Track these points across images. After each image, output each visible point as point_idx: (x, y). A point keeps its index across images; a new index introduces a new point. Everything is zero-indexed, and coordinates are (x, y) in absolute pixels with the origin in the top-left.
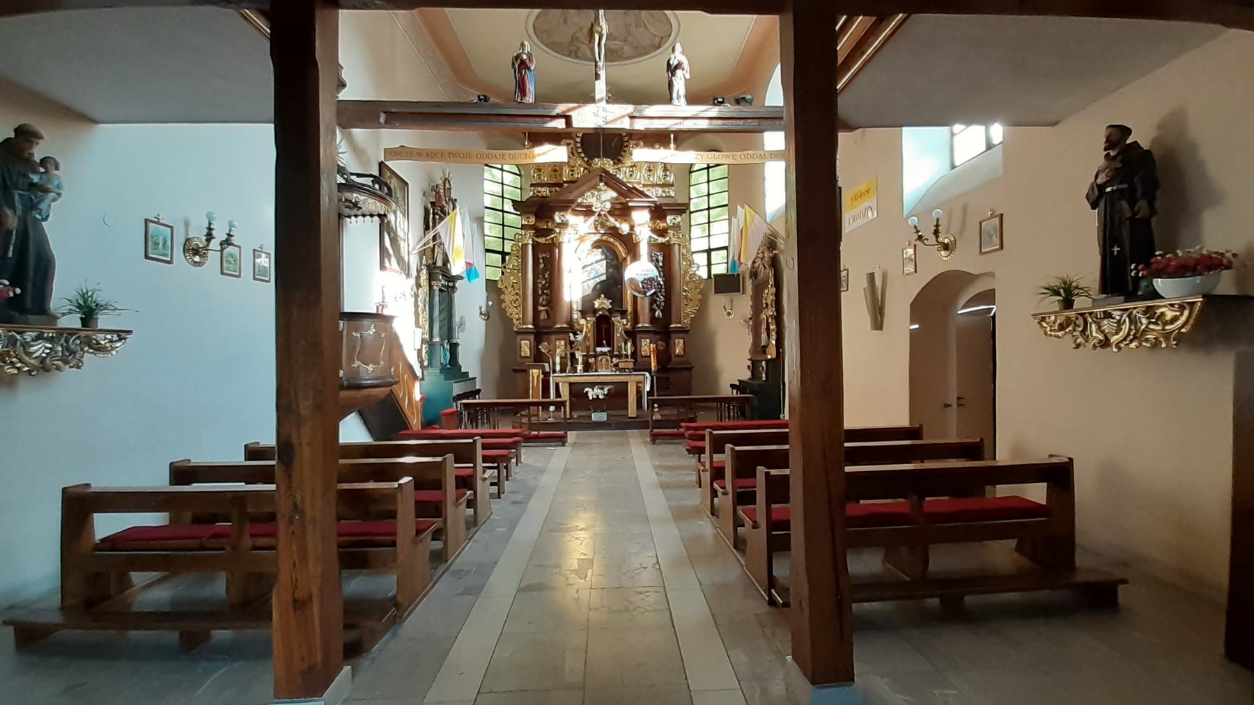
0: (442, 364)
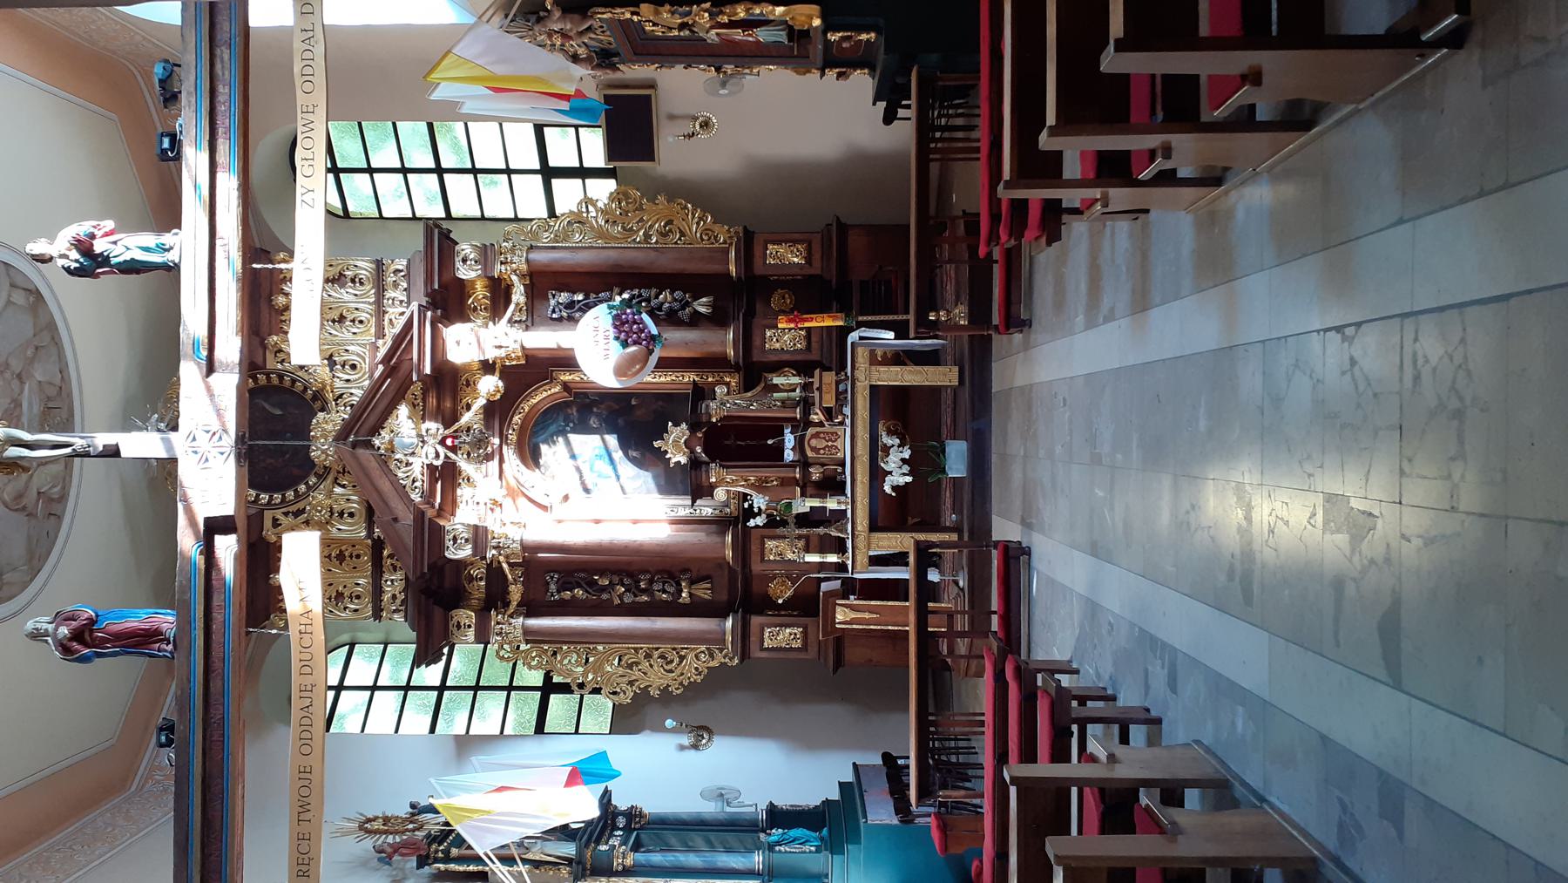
0: (818, 850)
